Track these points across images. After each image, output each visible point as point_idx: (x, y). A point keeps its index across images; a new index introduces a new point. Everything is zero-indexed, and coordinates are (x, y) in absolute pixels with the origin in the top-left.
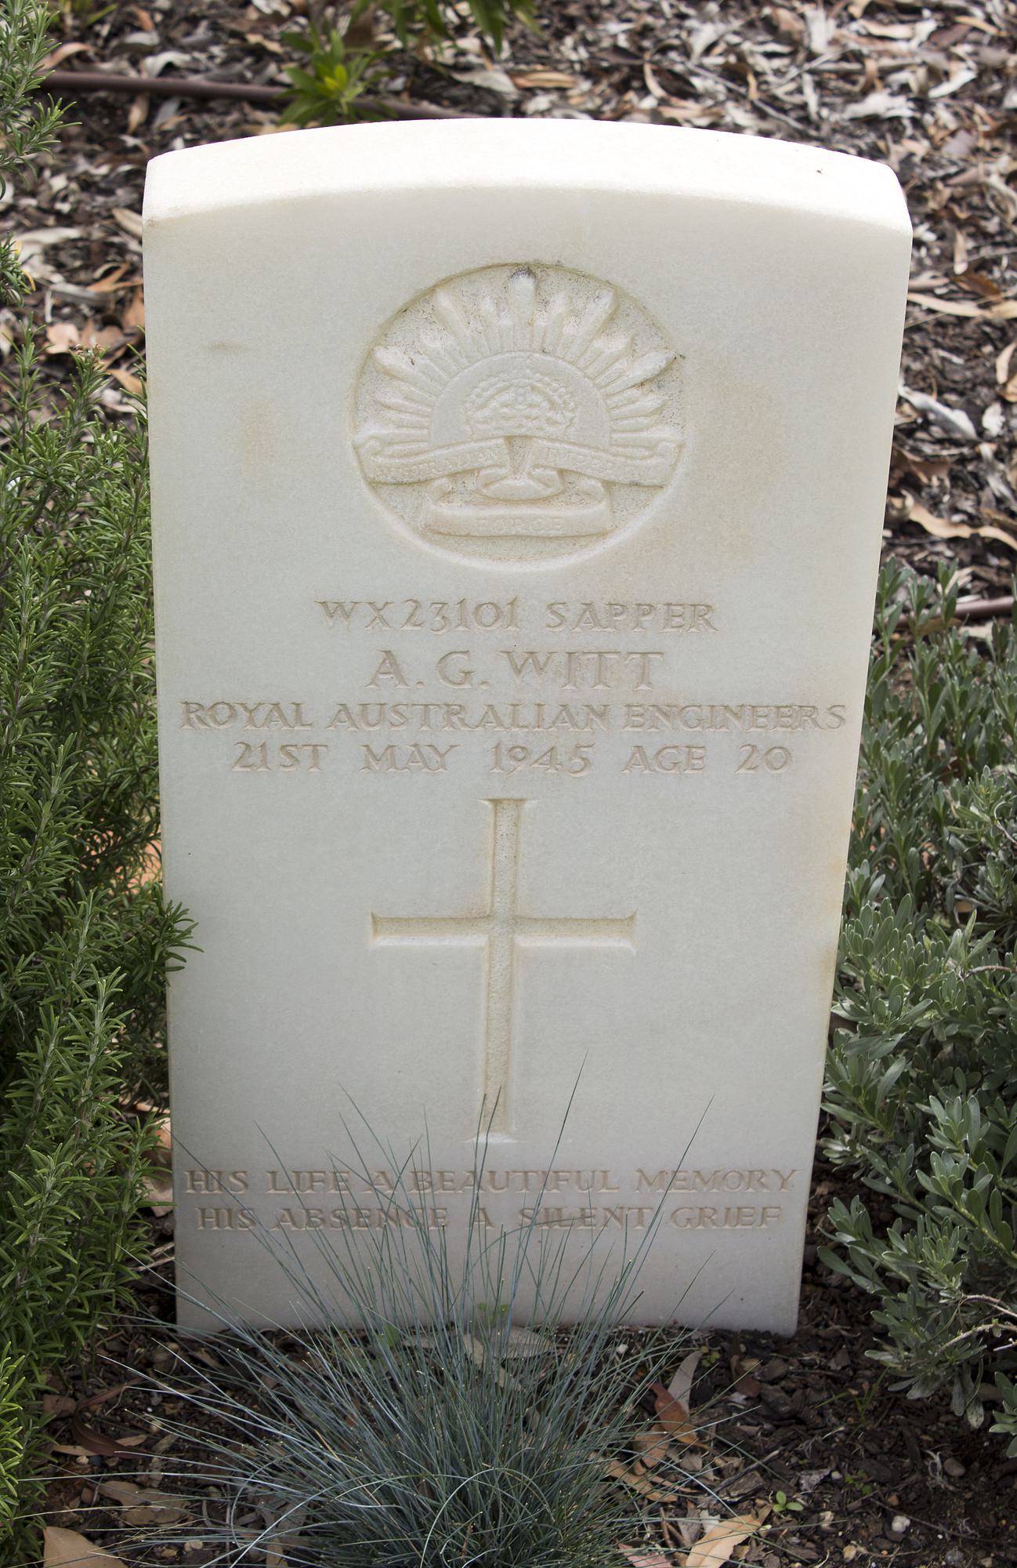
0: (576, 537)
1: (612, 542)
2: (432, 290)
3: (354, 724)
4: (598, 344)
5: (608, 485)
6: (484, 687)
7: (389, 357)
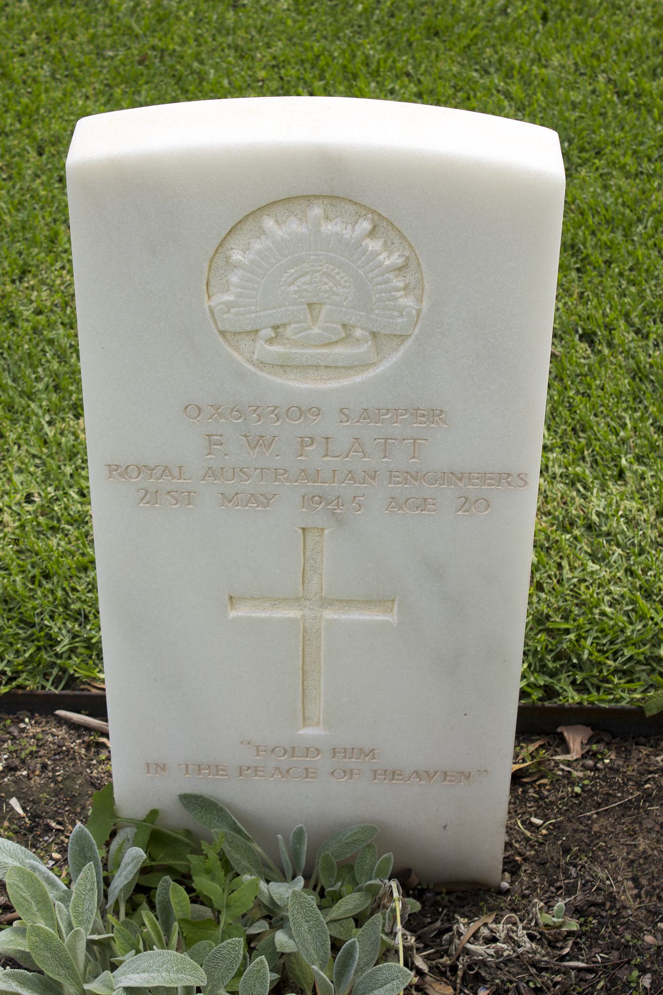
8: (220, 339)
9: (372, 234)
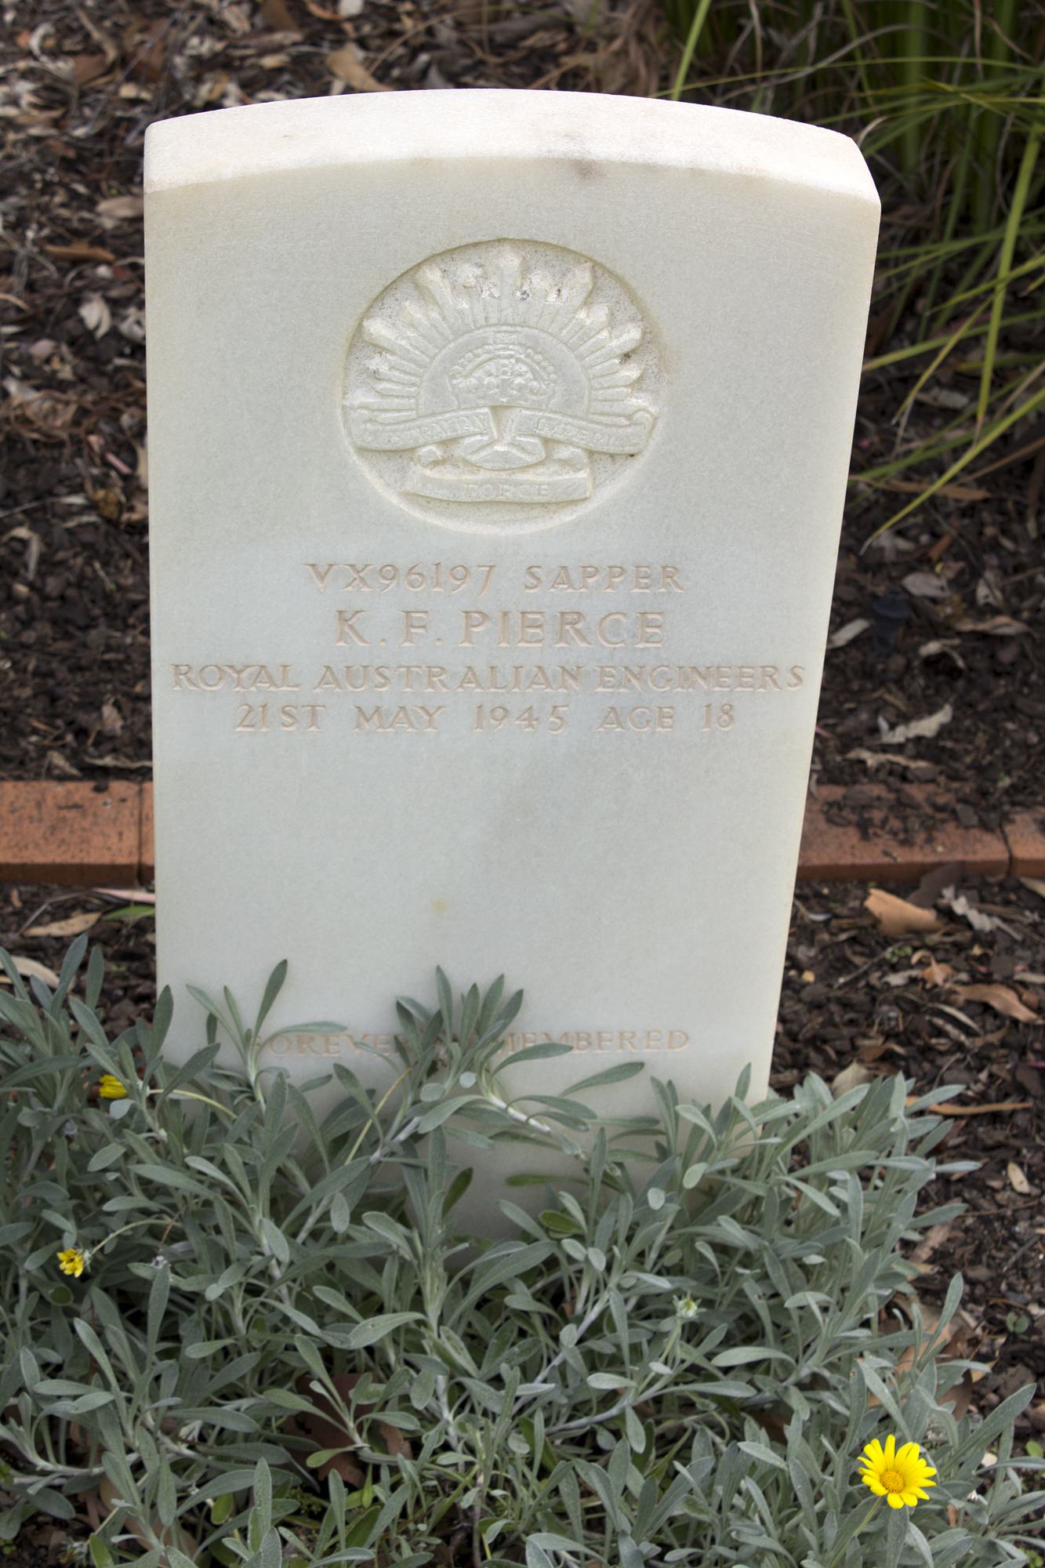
1: (589, 507)
3: (339, 685)
4: (582, 315)
5: (591, 453)
6: (383, 644)
7: (377, 328)
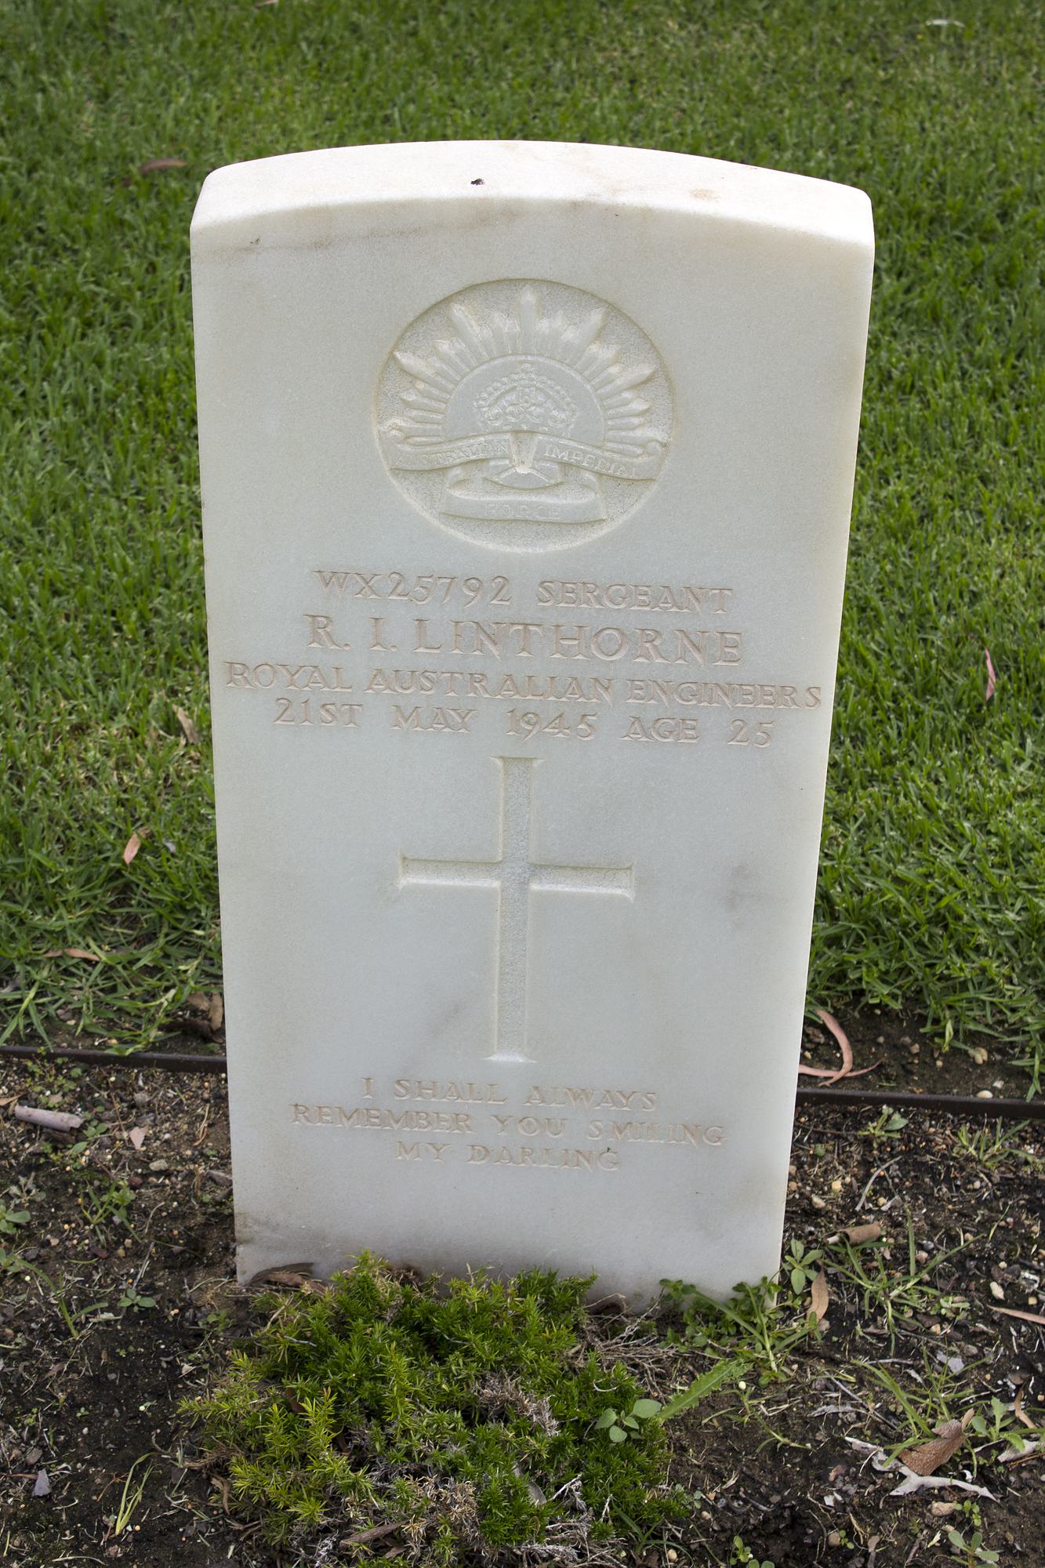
0: (584, 522)
2: (447, 300)
7: (406, 359)
8: (394, 481)
9: (600, 335)
